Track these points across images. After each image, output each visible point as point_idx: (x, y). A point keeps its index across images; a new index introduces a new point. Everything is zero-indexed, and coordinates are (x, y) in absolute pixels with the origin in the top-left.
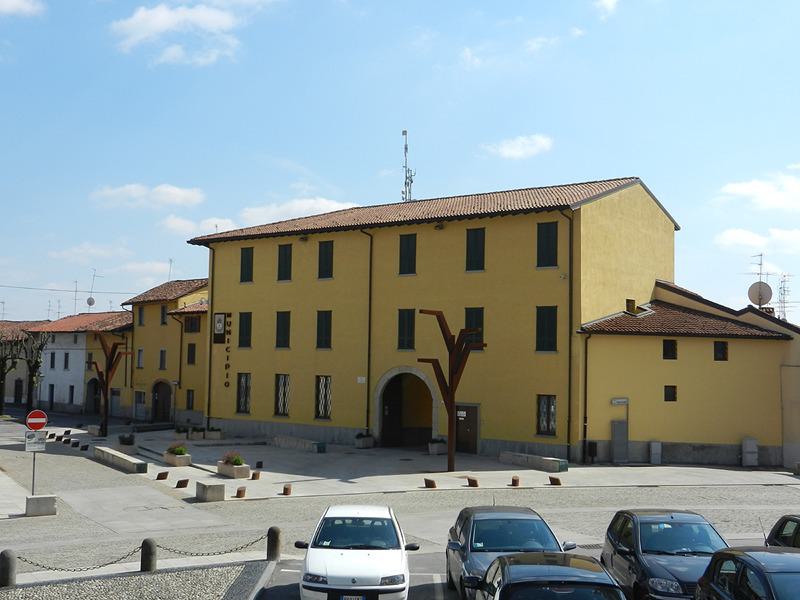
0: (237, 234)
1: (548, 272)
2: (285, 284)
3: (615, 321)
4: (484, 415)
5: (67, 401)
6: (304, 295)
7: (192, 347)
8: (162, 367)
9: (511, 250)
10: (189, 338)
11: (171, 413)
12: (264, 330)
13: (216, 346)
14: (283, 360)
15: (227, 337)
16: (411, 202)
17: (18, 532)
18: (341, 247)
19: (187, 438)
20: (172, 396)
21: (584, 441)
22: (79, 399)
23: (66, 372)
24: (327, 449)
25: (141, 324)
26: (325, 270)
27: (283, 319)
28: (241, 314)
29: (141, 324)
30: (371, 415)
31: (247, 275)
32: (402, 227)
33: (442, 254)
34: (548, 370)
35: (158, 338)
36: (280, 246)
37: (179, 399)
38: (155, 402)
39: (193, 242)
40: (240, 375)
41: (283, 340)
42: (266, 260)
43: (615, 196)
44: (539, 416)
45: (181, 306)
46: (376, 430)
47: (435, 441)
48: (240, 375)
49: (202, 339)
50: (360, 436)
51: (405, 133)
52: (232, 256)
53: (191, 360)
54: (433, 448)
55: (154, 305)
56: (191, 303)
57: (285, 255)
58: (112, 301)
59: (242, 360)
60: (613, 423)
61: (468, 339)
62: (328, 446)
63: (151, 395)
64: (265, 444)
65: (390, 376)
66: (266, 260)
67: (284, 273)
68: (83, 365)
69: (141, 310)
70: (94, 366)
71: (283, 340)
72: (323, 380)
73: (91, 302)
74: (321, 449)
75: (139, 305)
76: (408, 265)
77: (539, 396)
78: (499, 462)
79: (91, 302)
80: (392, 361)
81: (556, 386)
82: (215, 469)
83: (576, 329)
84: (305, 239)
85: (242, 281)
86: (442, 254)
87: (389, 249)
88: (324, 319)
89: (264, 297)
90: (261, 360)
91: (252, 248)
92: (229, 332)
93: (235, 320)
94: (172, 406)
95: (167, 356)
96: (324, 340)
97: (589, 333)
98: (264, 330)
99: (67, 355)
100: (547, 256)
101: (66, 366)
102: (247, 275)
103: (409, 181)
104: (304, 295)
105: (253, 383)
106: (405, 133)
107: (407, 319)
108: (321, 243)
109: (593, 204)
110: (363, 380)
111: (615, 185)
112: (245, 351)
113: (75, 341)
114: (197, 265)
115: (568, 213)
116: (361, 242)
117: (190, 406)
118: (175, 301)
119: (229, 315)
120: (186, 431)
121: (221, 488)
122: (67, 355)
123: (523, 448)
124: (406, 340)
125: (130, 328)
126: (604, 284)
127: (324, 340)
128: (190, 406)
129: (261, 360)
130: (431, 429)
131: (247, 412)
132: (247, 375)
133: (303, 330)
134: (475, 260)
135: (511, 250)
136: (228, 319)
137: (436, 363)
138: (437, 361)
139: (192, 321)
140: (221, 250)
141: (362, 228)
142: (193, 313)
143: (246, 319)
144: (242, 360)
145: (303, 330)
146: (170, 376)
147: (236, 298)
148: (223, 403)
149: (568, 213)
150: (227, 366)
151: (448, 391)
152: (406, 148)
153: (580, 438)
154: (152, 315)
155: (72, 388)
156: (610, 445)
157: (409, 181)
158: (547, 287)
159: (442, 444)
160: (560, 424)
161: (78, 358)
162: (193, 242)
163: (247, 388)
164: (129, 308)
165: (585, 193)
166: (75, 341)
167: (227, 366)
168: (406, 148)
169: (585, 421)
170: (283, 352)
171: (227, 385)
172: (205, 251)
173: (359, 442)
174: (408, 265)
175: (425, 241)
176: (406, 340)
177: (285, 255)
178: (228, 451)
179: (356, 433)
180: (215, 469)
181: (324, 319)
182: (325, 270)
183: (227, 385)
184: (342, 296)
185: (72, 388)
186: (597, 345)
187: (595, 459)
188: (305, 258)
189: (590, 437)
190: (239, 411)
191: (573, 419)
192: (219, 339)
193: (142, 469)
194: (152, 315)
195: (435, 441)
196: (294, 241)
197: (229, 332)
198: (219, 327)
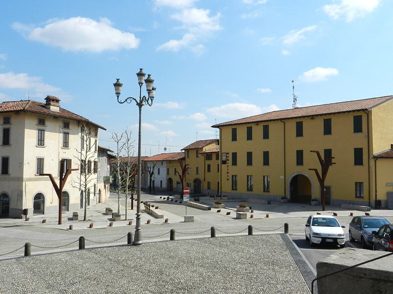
0: (225, 124)
1: (359, 135)
2: (250, 141)
3: (387, 153)
4: (333, 190)
5: (160, 186)
6: (258, 145)
7: (209, 166)
8: (197, 173)
9: (343, 128)
10: (208, 162)
11: (202, 191)
12: (242, 159)
13: (223, 165)
14: (250, 170)
15: (227, 162)
16: (296, 108)
17: (10, 248)
18: (272, 128)
19: (214, 199)
20: (202, 184)
21: (376, 200)
22: (164, 185)
23: (159, 176)
24: (116, 220)
25: (188, 157)
26: (266, 136)
27: (250, 155)
28: (233, 153)
29: (188, 157)
30: (286, 190)
31: (234, 138)
32: (340, 114)
33: (314, 130)
34: (360, 174)
35: (193, 162)
36: (324, 120)
37: (204, 185)
38: (195, 187)
39: (213, 127)
40: (233, 176)
41: (250, 162)
42: (242, 133)
43: (385, 103)
44: (356, 190)
45: (204, 150)
46: (288, 196)
47: (313, 200)
48: (233, 176)
49: (214, 163)
50: (282, 198)
51: (293, 81)
52: (228, 132)
53: (209, 170)
54: (313, 203)
55: (194, 150)
56: (207, 149)
57: (234, 132)
58: (176, 147)
59: (233, 170)
60: (388, 193)
61: (327, 160)
62: (271, 202)
63: (193, 184)
64: (244, 201)
65: (294, 175)
66: (242, 133)
67: (249, 137)
68: (165, 172)
69: (188, 152)
70: (177, 173)
71: (250, 162)
72: (266, 177)
73: (165, 149)
74: (269, 203)
75: (187, 150)
76: (300, 133)
77: (356, 182)
78: (341, 208)
79: (165, 149)
80: (294, 170)
81: (363, 178)
82: (236, 209)
83: (371, 157)
84: (257, 125)
85: (264, 138)
86: (314, 130)
87: (292, 127)
88: (266, 155)
89: (242, 146)
90: (241, 170)
91: (236, 129)
92: (228, 160)
93: (230, 156)
94: (202, 188)
95: (157, 173)
96: (266, 162)
97: (376, 158)
98: (242, 159)
99: (159, 169)
100: (358, 128)
101: (159, 173)
102: (234, 138)
103: (295, 100)
104: (258, 145)
105: (238, 179)
106: (293, 81)
107: (300, 154)
108: (264, 126)
109: (377, 108)
110: (283, 177)
111: (384, 99)
112: (234, 167)
113: (162, 164)
114: (215, 134)
115: (367, 112)
116: (281, 124)
117: (209, 188)
118: (202, 149)
119: (228, 154)
120: (213, 197)
121: (246, 214)
122: (159, 169)
123: (350, 203)
124: (300, 160)
125: (184, 159)
126: (382, 139)
127: (266, 162)
128: (209, 188)
129: (241, 170)
130: (311, 196)
131: (236, 189)
132: (236, 176)
133: (258, 159)
134: (328, 130)
135: (343, 128)
136: (227, 155)
137: (316, 171)
138: (316, 170)
139: (209, 156)
140: (224, 129)
141: (281, 119)
142: (210, 153)
143: (234, 155)
144: (233, 170)
145: (258, 159)
146: (201, 176)
147: (230, 147)
148: (227, 187)
149: (367, 112)
150: (228, 173)
151: (321, 181)
152: (294, 87)
153: (374, 199)
154: (193, 154)
155: (161, 181)
156: (387, 202)
157: (295, 100)
158: (358, 140)
159: (316, 201)
160: (365, 193)
161: (163, 170)
162: (213, 127)
163: (236, 181)
164: (183, 151)
165: (372, 103)
166: (162, 164)
167: (228, 173)
168: (294, 87)
169: (376, 192)
170: (250, 167)
171: (228, 179)
172: (218, 130)
173: (283, 201)
174: (300, 133)
175: (306, 125)
176: (300, 160)
177: (234, 132)
178: (241, 203)
179: (281, 197)
180: (236, 209)
181: (266, 155)
182: (266, 136)
183: (228, 179)
184: (273, 145)
185: (161, 181)
186: (380, 163)
187: (381, 207)
188: (258, 132)
189: (378, 198)
190: (233, 189)
191: (371, 192)
192: (224, 162)
193: (209, 209)
194: (193, 154)
195: (313, 200)
196: (254, 126)
197: (228, 160)
198: (224, 158)
